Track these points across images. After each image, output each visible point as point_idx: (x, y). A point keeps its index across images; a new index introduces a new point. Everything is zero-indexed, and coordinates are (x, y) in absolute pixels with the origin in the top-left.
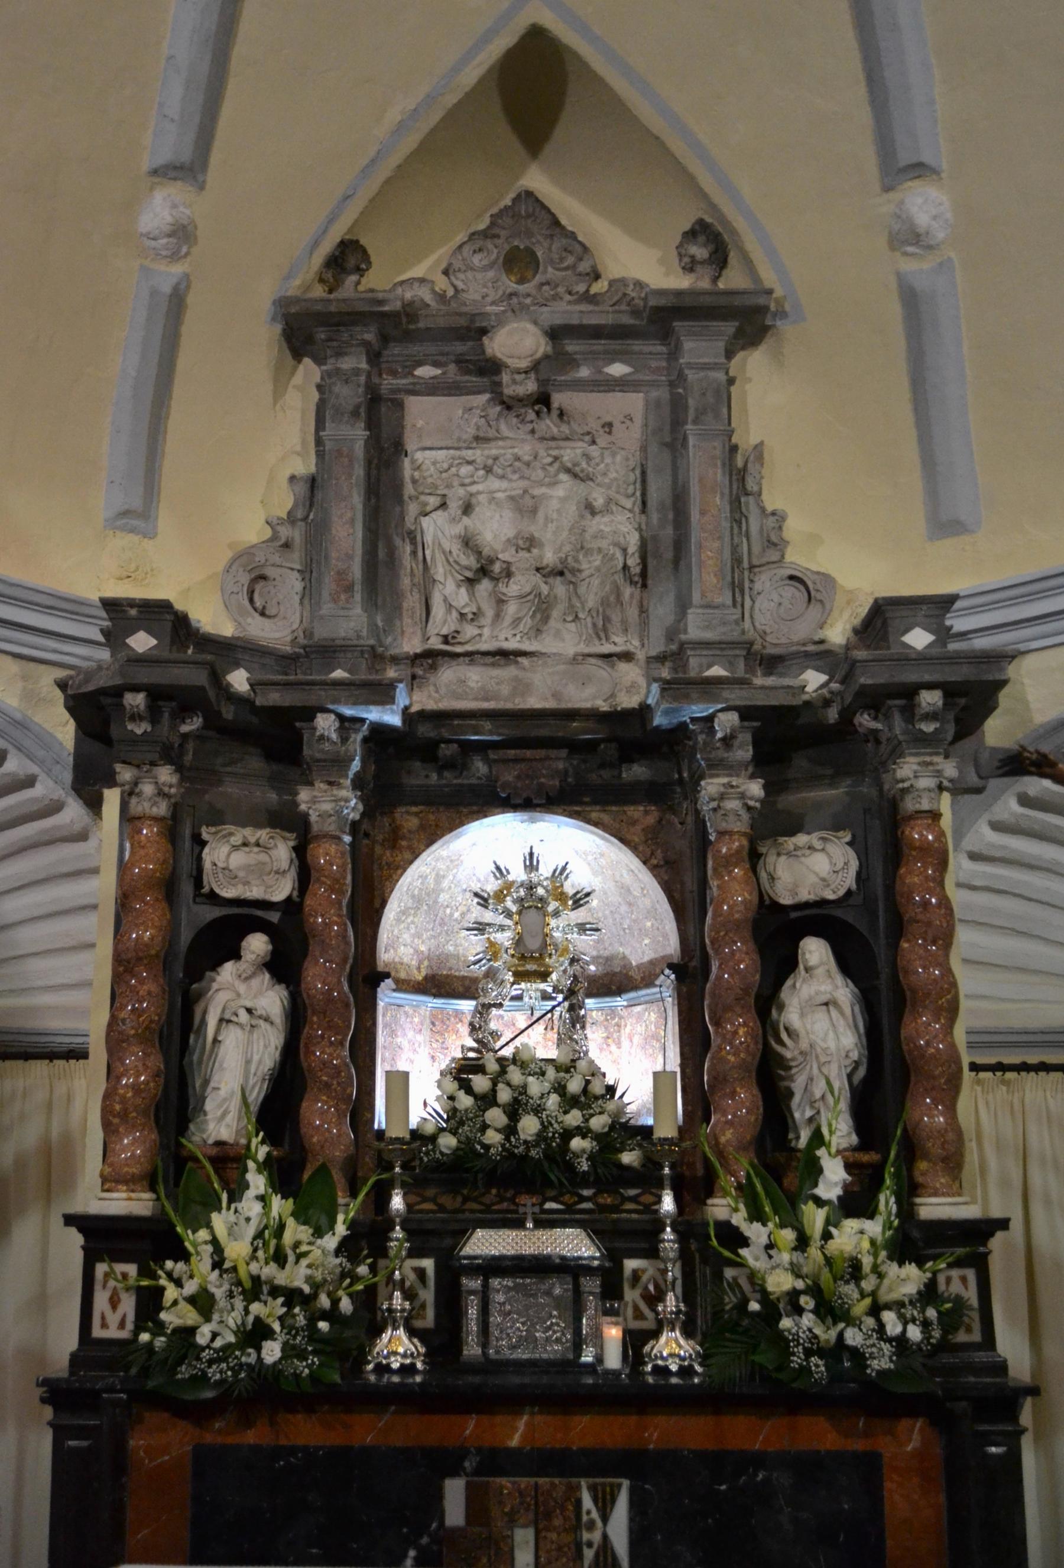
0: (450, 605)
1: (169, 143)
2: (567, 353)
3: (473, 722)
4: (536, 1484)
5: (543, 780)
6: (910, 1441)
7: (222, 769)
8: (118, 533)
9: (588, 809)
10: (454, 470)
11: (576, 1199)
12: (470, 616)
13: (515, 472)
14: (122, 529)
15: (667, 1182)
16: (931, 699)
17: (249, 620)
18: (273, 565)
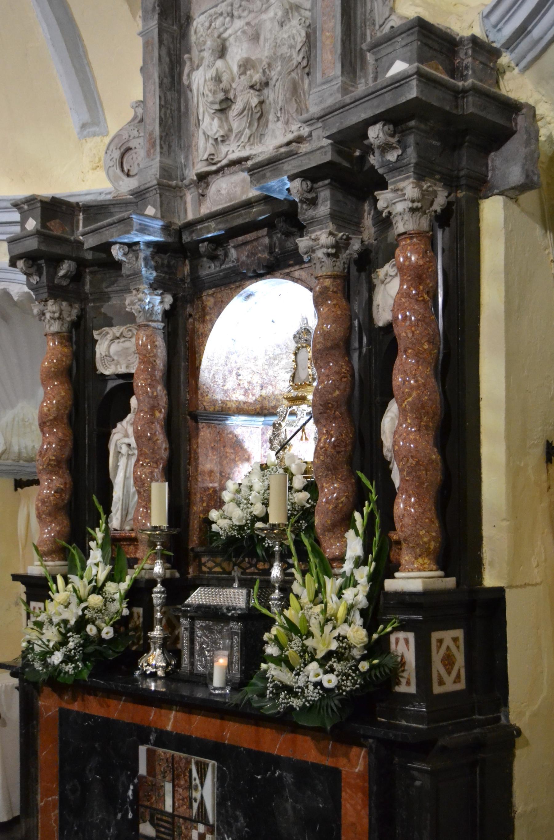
0: (208, 136)
3: (206, 224)
4: (173, 756)
5: (260, 255)
6: (357, 764)
7: (106, 290)
8: (88, 140)
9: (293, 269)
11: (286, 566)
13: (244, 10)
14: (88, 136)
15: (277, 557)
18: (134, 138)
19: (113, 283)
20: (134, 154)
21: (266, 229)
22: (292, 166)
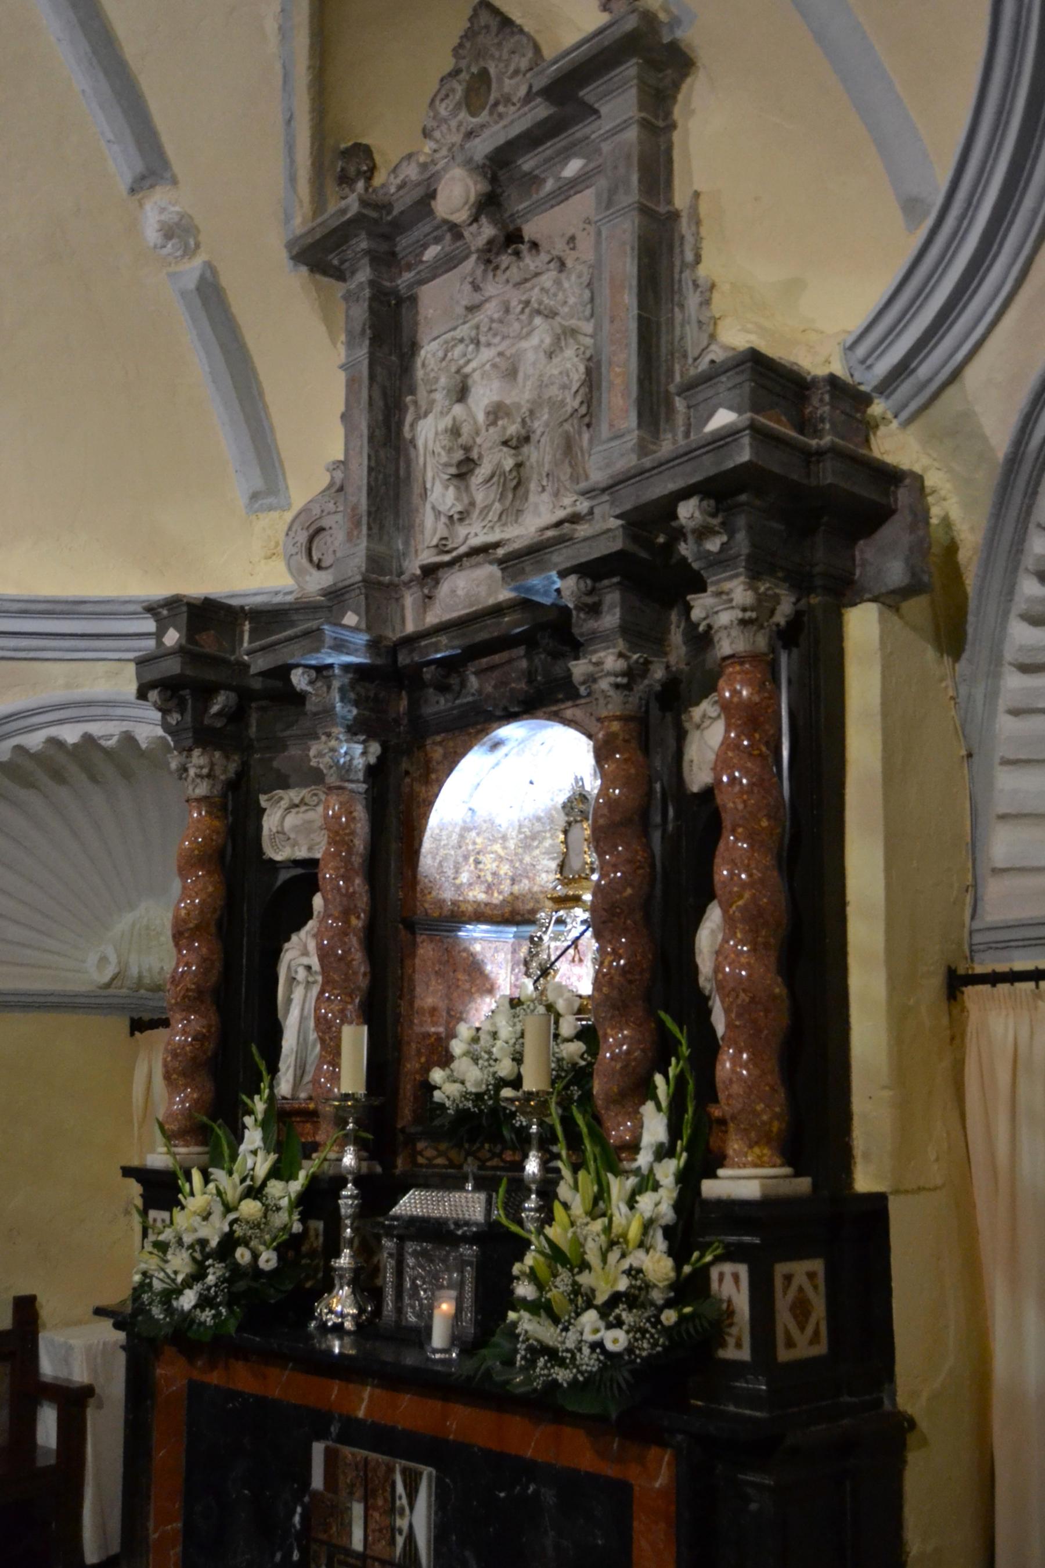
1: (120, 165)
2: (526, 174)
3: (434, 640)
4: (366, 1459)
5: (513, 685)
7: (281, 735)
9: (563, 706)
10: (449, 354)
11: (548, 1156)
12: (456, 517)
13: (495, 335)
15: (535, 1142)
16: (688, 512)
17: (308, 578)
19: (289, 726)
20: (328, 537)
21: (523, 647)
22: (563, 557)
